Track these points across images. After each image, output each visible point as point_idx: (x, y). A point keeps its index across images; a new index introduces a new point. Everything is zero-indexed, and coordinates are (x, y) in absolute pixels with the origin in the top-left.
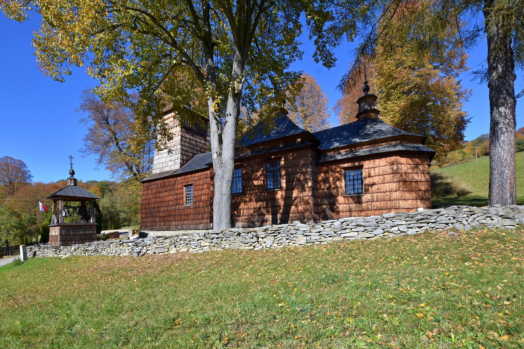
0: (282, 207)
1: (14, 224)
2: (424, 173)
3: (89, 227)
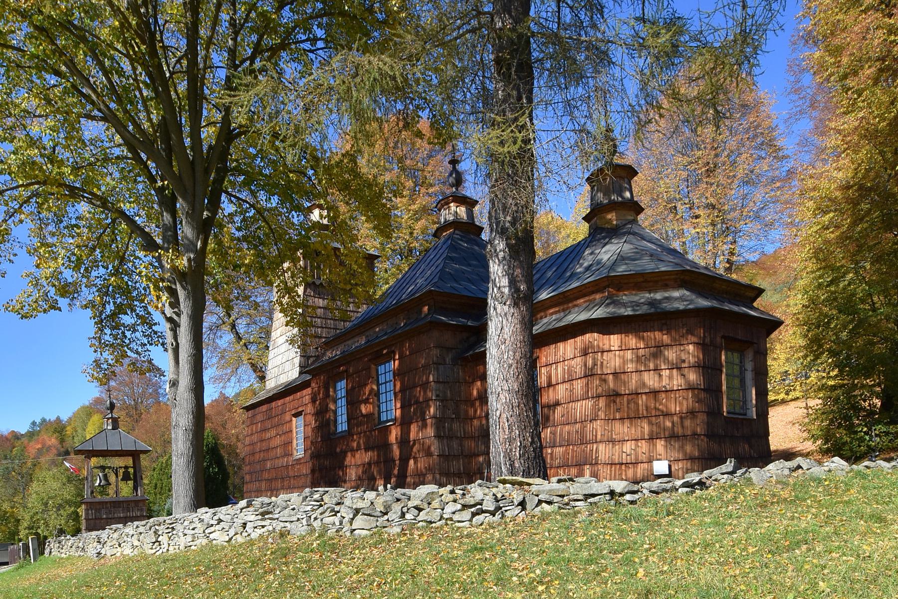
0: (397, 462)
1: (68, 497)
2: (679, 369)
3: (133, 505)
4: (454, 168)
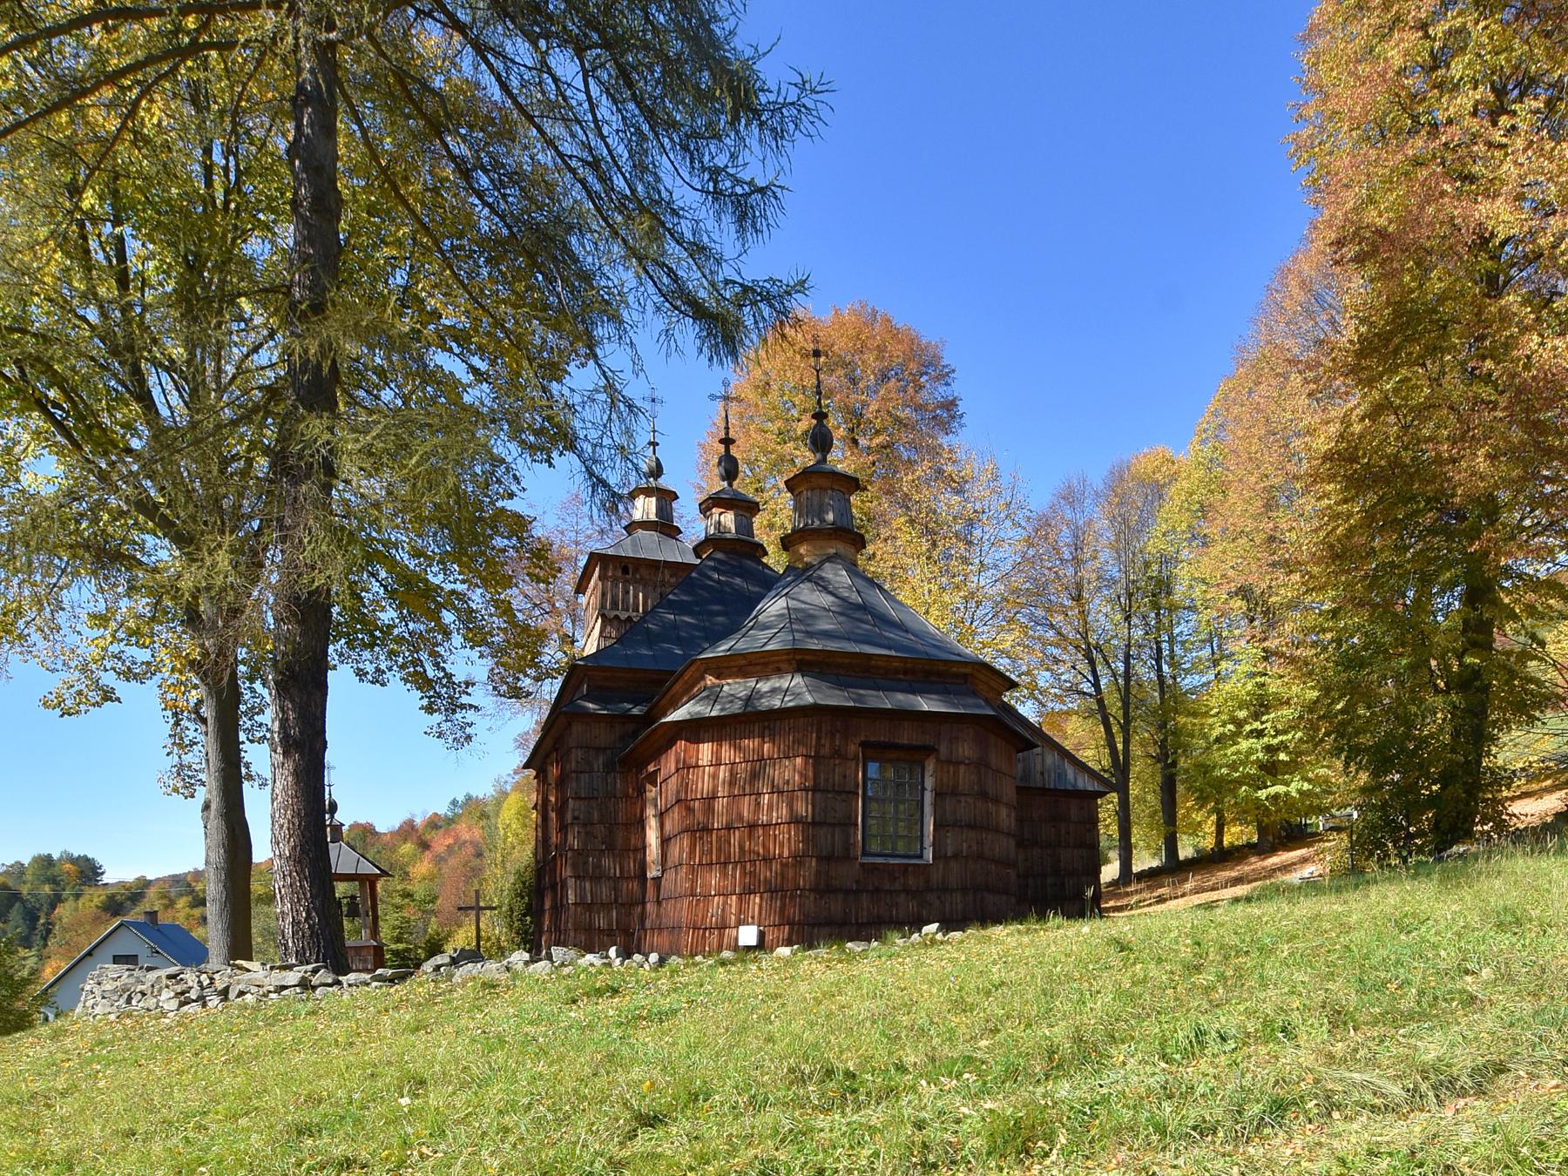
4: (727, 450)
